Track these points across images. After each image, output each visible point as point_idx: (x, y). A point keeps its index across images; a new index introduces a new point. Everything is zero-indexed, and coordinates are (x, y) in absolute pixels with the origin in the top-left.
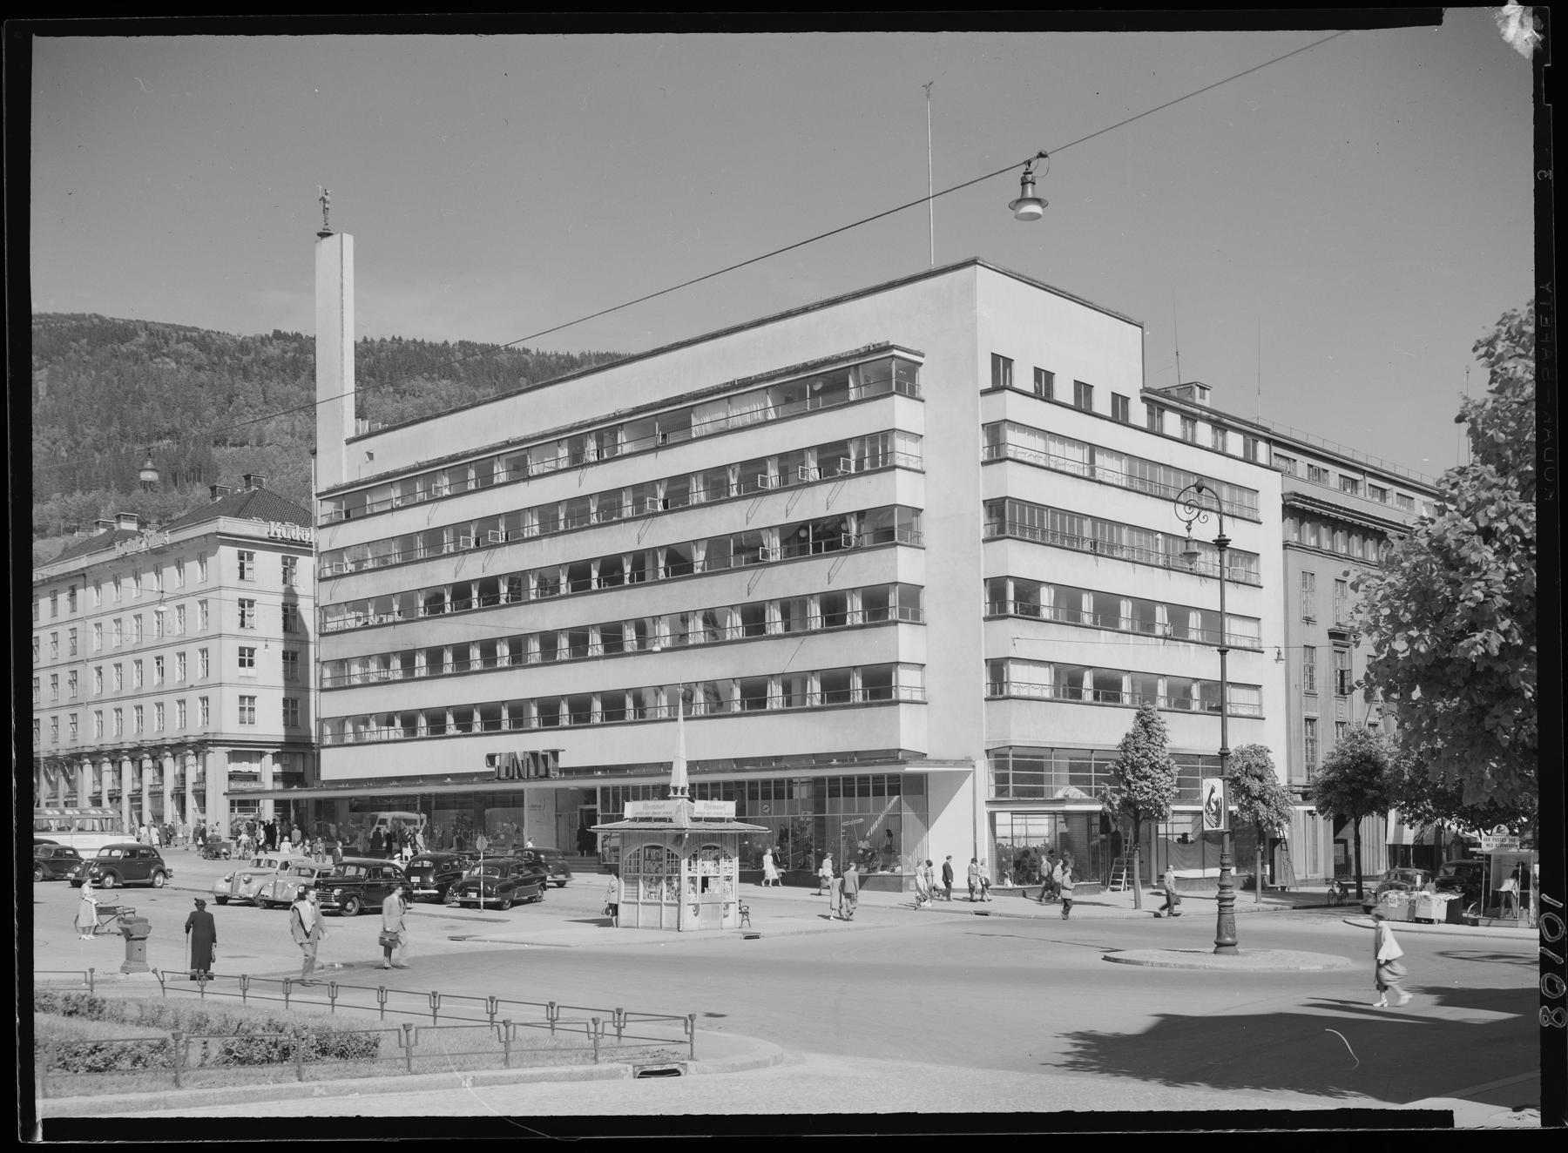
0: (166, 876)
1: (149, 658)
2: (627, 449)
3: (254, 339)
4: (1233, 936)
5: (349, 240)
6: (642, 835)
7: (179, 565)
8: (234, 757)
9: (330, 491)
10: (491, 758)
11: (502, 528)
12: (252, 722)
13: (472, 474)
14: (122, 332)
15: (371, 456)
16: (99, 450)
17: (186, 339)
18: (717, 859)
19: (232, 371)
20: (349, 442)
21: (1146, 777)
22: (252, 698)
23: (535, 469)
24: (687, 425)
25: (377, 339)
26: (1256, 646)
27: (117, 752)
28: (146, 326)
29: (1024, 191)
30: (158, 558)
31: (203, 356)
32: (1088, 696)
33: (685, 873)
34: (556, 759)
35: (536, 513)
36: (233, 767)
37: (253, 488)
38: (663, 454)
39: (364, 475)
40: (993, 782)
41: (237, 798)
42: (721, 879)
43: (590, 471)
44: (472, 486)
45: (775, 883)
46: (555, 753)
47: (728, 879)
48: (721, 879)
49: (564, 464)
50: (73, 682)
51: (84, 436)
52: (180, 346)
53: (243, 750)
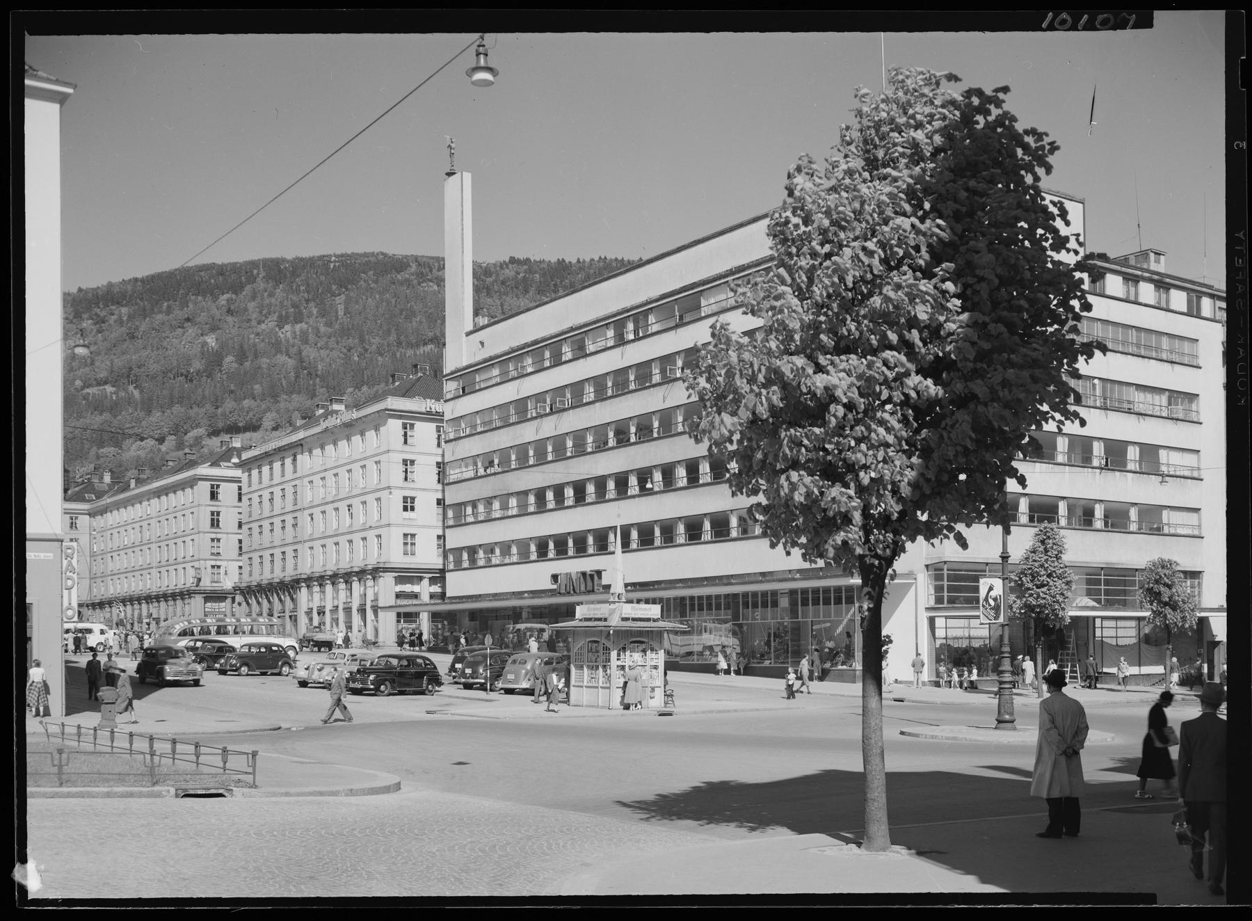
0: (291, 667)
1: (343, 506)
2: (655, 328)
3: (495, 265)
4: (1012, 714)
5: (467, 177)
6: (587, 632)
7: (362, 434)
8: (399, 580)
9: (452, 373)
10: (555, 578)
11: (568, 395)
12: (413, 554)
13: (547, 354)
14: (399, 264)
15: (482, 344)
16: (381, 355)
18: (644, 651)
20: (468, 334)
21: (1043, 586)
22: (413, 536)
23: (591, 348)
24: (699, 307)
25: (588, 260)
26: (1195, 474)
27: (322, 577)
28: (416, 259)
29: (478, 61)
30: (349, 429)
32: (1099, 524)
33: (614, 662)
34: (600, 578)
35: (592, 382)
36: (399, 588)
37: (420, 374)
38: (681, 331)
40: (932, 591)
41: (402, 610)
42: (648, 668)
43: (629, 347)
44: (547, 364)
45: (727, 672)
46: (599, 573)
47: (656, 667)
48: (648, 668)
49: (611, 343)
50: (295, 526)
51: (370, 344)
53: (406, 575)
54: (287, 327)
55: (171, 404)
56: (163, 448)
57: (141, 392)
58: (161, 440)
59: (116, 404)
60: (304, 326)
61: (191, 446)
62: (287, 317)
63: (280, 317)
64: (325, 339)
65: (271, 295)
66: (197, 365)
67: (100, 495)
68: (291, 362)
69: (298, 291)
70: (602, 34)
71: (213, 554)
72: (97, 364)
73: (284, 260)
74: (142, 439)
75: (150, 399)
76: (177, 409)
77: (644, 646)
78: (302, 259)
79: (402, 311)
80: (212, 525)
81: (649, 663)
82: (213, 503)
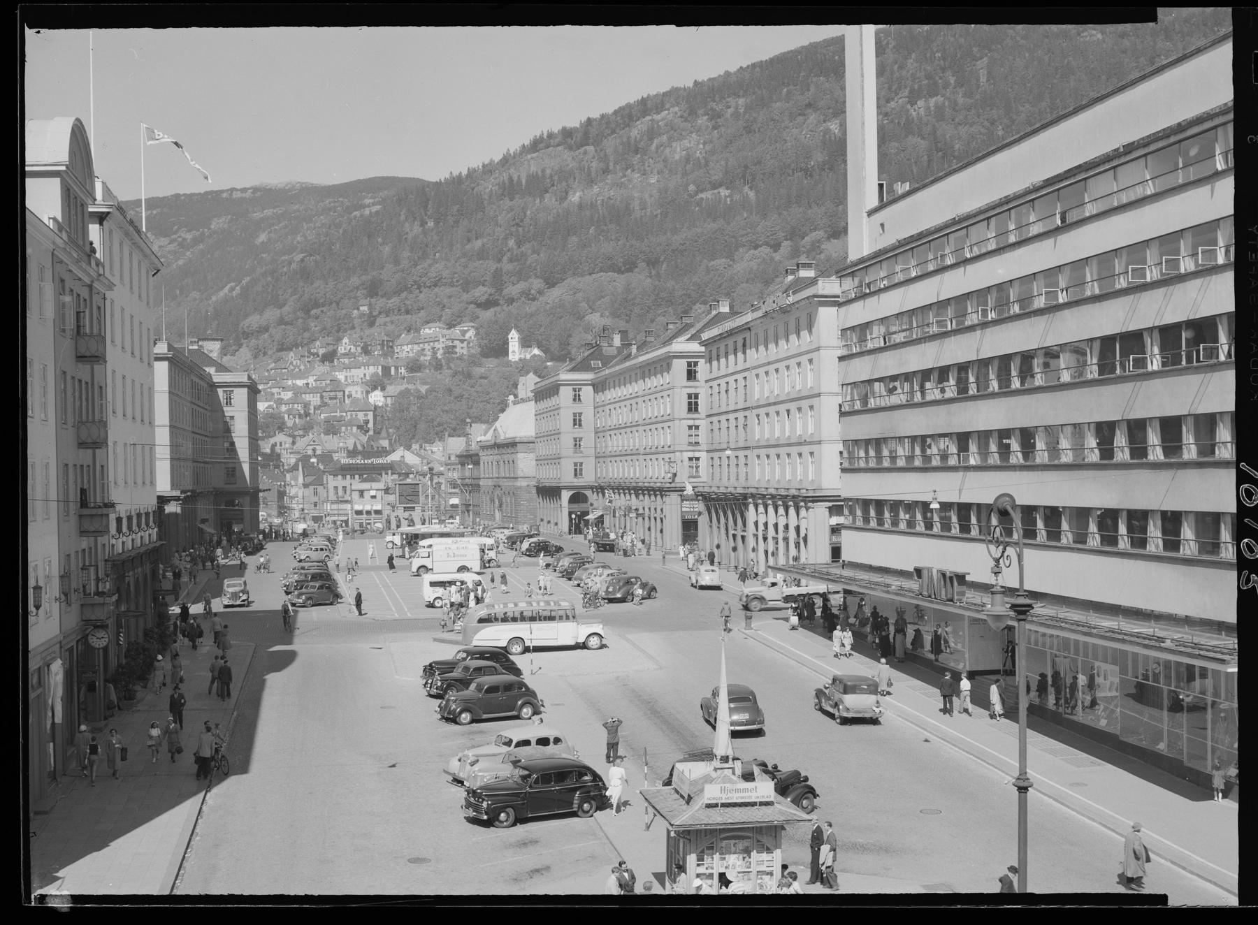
54: (921, 103)
57: (757, 192)
58: (776, 247)
60: (940, 99)
63: (912, 91)
65: (901, 68)
68: (923, 144)
71: (690, 444)
72: (712, 164)
74: (756, 247)
80: (690, 410)
81: (755, 868)
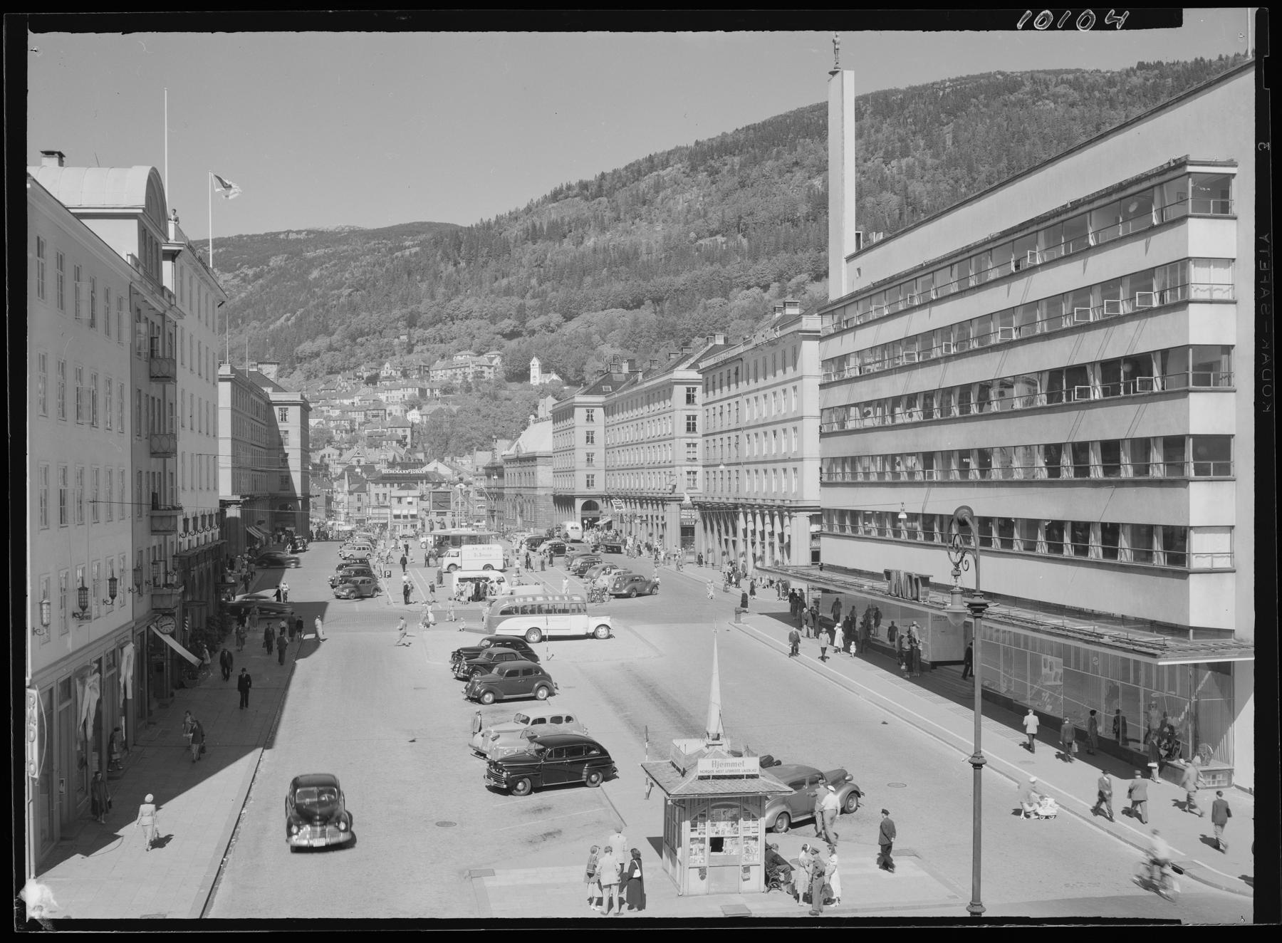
17: (1063, 82)
19: (1100, 103)
25: (1232, 55)
31: (1076, 95)
39: (857, 288)
42: (741, 840)
48: (741, 840)
51: (979, 173)
52: (1058, 89)
54: (894, 163)
55: (776, 251)
56: (767, 296)
57: (749, 240)
58: (766, 288)
59: (726, 253)
60: (910, 160)
61: (794, 293)
62: (893, 152)
63: (886, 153)
64: (932, 171)
65: (877, 131)
66: (803, 209)
67: (616, 386)
69: (905, 124)
70: (589, 33)
72: (710, 215)
73: (897, 91)
74: (748, 288)
75: (757, 247)
76: (783, 256)
77: (735, 811)
78: (915, 88)
79: (1014, 134)
80: (688, 430)
81: (742, 834)
82: (689, 407)
